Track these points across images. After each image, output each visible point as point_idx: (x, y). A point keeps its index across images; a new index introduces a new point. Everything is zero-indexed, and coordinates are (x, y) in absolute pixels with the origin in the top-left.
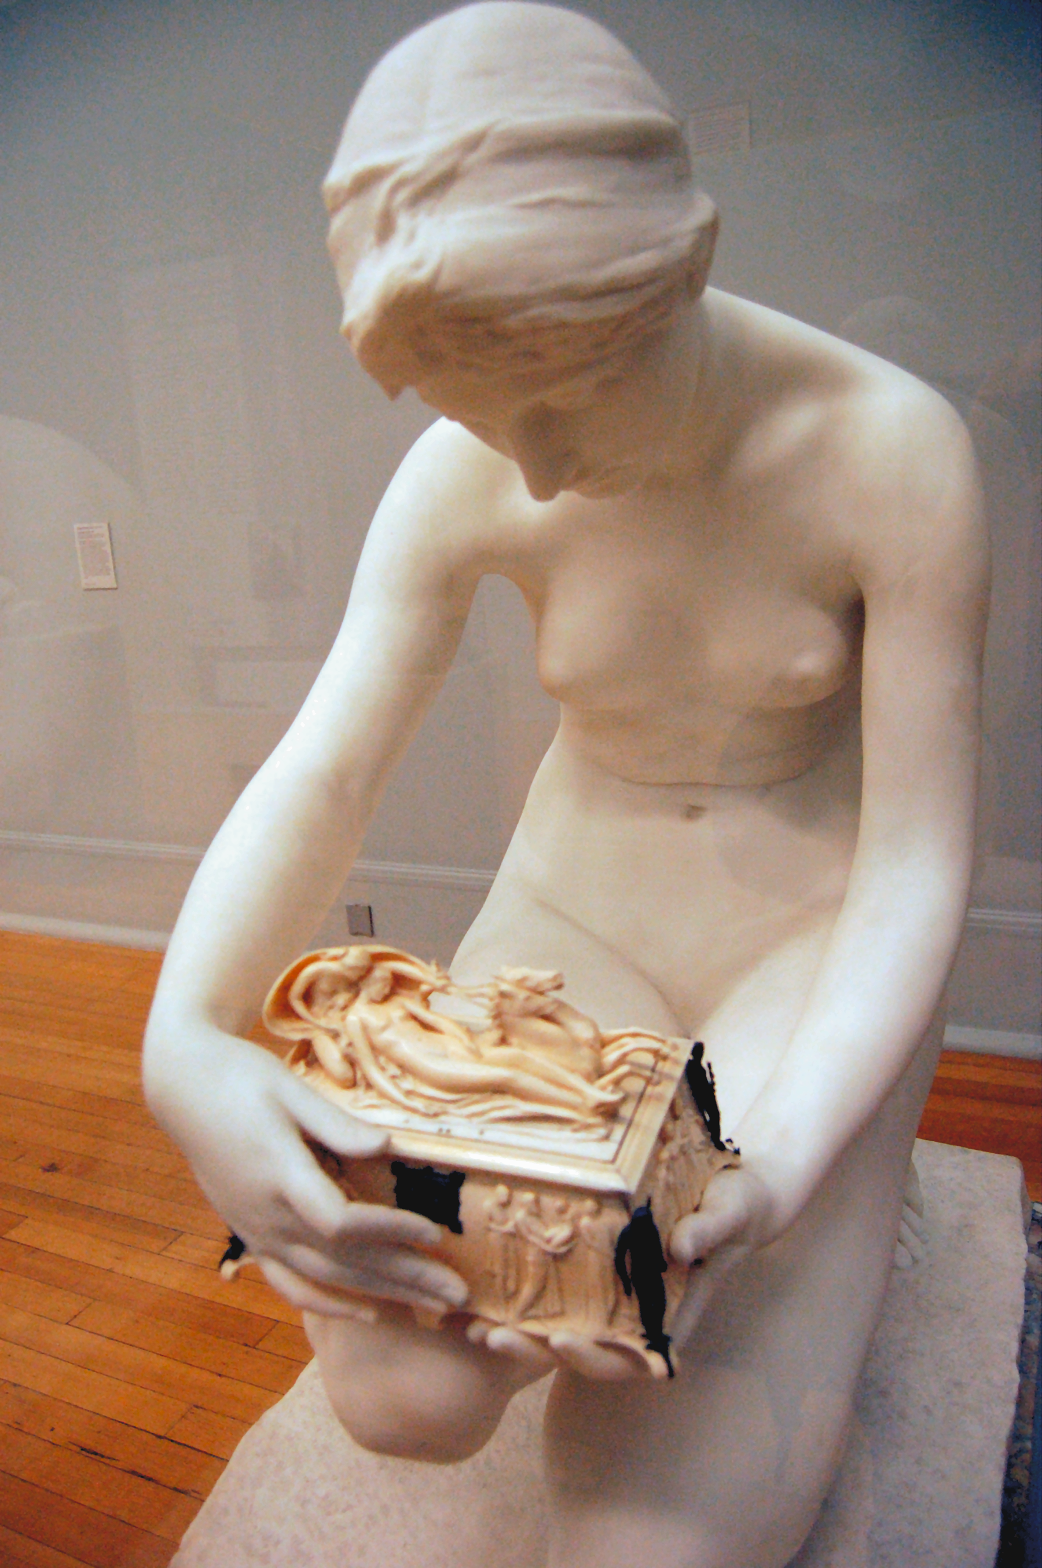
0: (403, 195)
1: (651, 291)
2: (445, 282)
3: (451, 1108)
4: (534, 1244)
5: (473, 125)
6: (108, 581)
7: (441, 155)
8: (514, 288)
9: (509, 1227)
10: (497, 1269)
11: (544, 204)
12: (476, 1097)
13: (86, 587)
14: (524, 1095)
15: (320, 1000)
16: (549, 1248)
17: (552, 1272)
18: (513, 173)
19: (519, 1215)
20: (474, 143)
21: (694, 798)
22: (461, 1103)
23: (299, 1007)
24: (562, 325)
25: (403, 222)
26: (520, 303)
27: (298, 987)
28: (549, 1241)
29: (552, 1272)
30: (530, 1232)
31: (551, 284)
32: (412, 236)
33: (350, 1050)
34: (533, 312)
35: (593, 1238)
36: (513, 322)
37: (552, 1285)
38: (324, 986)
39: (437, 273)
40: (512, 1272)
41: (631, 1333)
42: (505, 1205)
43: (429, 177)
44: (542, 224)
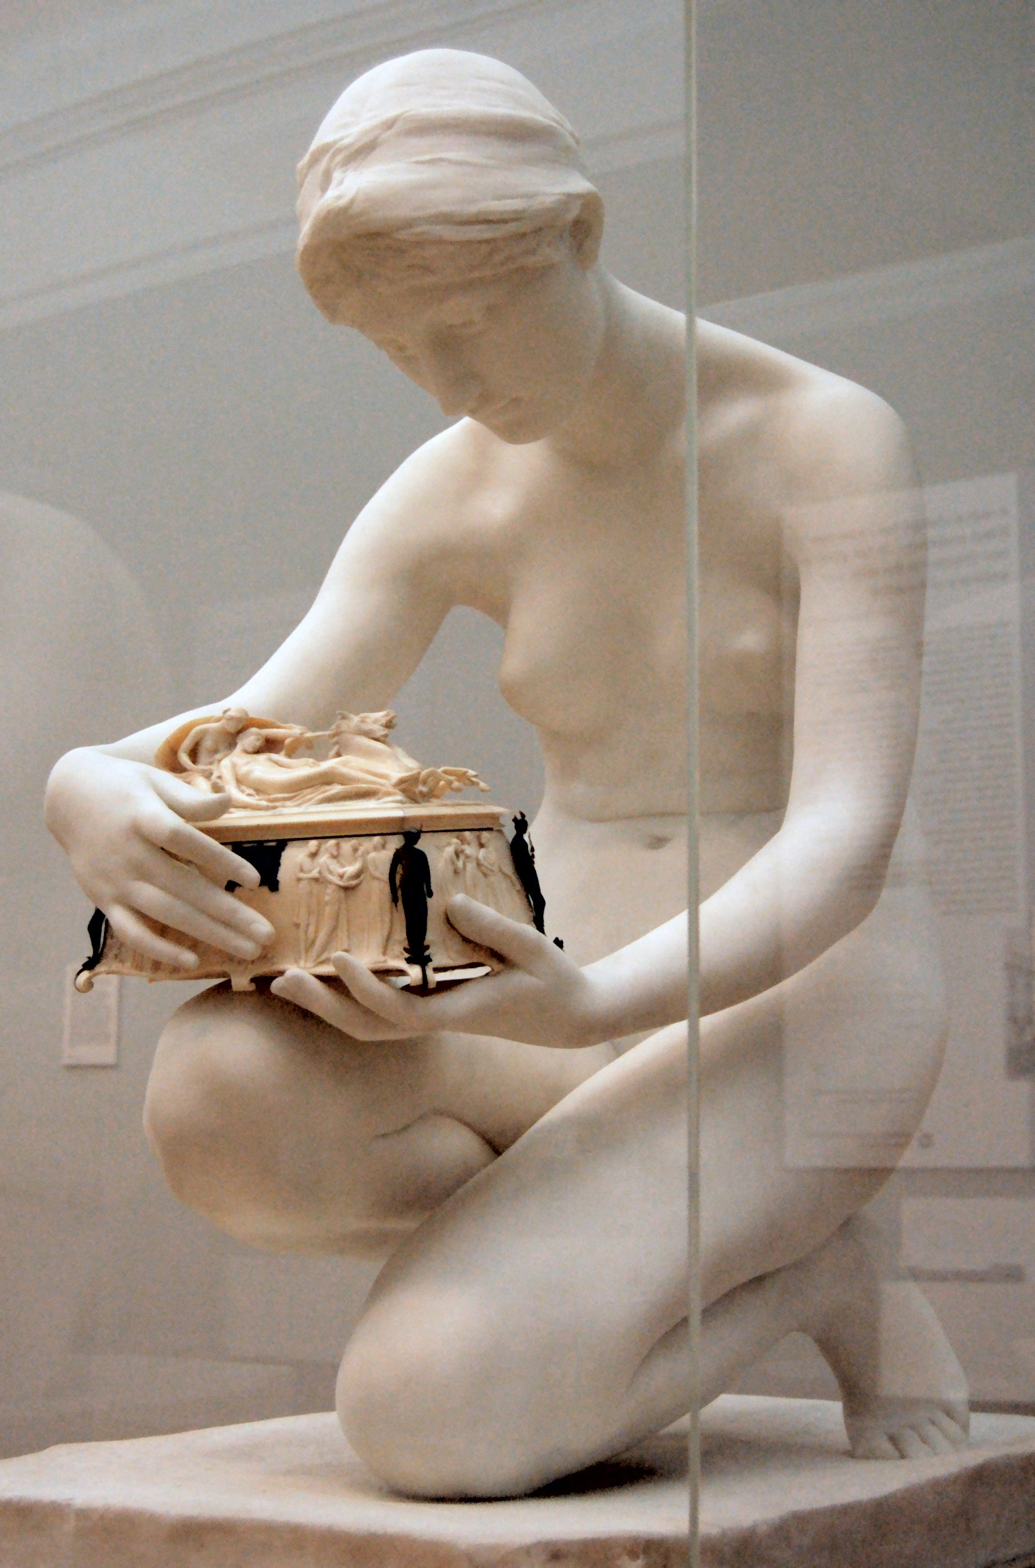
0: (339, 158)
1: (512, 227)
2: (356, 209)
3: (288, 803)
4: (330, 883)
5: (391, 113)
6: (105, 1054)
7: (366, 132)
8: (404, 212)
9: (315, 873)
10: (302, 918)
11: (432, 162)
12: (309, 790)
13: (71, 1062)
14: (342, 779)
15: (203, 756)
16: (341, 883)
17: (344, 906)
18: (413, 141)
19: (323, 859)
20: (389, 124)
21: (658, 828)
22: (298, 797)
23: (184, 759)
24: (440, 242)
25: (337, 175)
26: (409, 223)
27: (187, 743)
28: (341, 876)
29: (344, 906)
30: (331, 872)
31: (433, 211)
32: (341, 182)
33: (219, 781)
34: (419, 229)
35: (376, 868)
36: (402, 235)
37: (343, 921)
38: (208, 743)
39: (352, 202)
40: (313, 919)
41: (397, 957)
42: (314, 855)
43: (356, 146)
44: (426, 174)
